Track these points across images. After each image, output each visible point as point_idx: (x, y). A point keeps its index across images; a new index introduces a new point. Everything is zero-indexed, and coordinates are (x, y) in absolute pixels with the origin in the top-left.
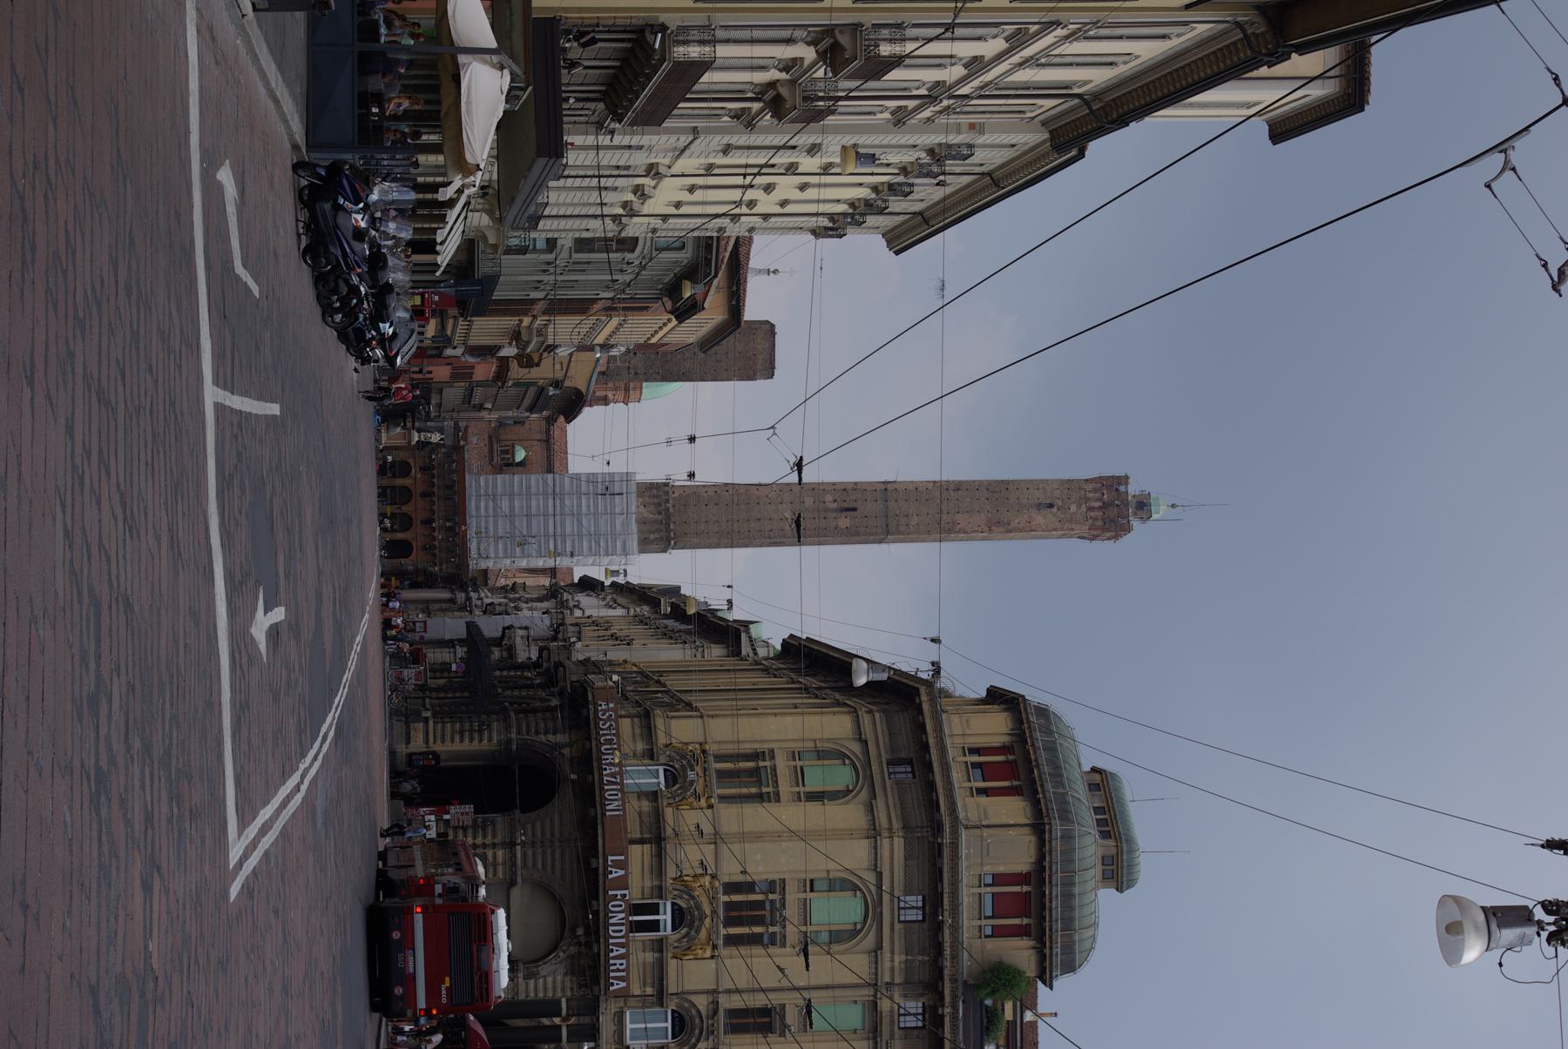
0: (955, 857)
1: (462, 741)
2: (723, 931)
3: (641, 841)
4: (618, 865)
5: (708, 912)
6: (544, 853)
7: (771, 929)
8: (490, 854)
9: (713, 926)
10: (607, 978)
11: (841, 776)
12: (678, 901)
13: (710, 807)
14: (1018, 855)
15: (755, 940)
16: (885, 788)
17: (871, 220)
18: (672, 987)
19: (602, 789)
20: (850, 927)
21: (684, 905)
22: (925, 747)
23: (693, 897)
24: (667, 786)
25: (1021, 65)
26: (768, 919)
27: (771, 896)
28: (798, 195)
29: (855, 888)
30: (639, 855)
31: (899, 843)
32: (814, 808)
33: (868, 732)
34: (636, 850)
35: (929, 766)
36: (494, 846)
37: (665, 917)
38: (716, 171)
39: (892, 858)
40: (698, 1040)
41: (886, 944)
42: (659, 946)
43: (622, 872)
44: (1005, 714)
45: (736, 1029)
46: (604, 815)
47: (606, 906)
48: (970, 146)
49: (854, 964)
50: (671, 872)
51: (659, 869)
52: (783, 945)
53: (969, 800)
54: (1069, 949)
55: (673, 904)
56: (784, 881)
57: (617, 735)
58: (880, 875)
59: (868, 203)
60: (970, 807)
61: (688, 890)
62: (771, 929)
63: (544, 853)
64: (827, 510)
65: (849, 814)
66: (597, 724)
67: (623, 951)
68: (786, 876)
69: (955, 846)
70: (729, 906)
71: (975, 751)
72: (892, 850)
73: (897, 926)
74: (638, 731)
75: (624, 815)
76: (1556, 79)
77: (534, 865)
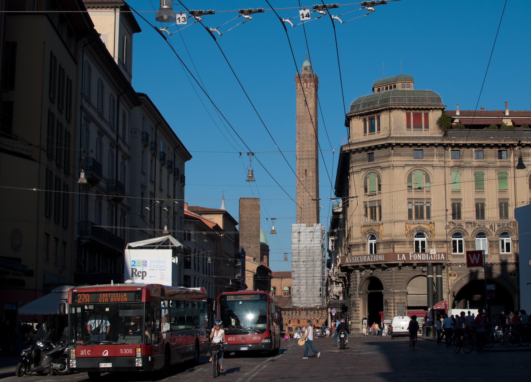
0: (400, 138)
1: (359, 310)
2: (425, 219)
3: (393, 248)
4: (401, 257)
5: (418, 225)
7: (425, 203)
8: (396, 301)
9: (424, 224)
10: (440, 260)
11: (373, 178)
12: (414, 235)
13: (382, 224)
14: (400, 116)
15: (428, 209)
16: (377, 163)
17: (178, 165)
18: (444, 238)
19: (375, 262)
20: (424, 176)
21: (416, 233)
22: (364, 149)
23: (413, 231)
24: (375, 239)
25: (101, 116)
26: (422, 204)
27: (413, 203)
28: (165, 192)
30: (398, 249)
31: (396, 158)
33: (359, 168)
34: (396, 250)
35: (370, 148)
36: (394, 299)
37: (420, 239)
38: (153, 220)
39: (400, 161)
40: (463, 229)
41: (430, 163)
42: (430, 242)
43: (404, 255)
45: (483, 217)
47: (415, 261)
48: (143, 133)
49: (437, 175)
50: (404, 238)
51: (403, 242)
53: (381, 133)
54: (432, 100)
55: (416, 237)
56: (475, 199)
57: (357, 256)
58: (407, 165)
59: (169, 167)
60: (383, 134)
61: (411, 232)
62: (425, 203)
63: (397, 282)
64: (306, 180)
65: (385, 175)
66: (353, 263)
68: (406, 198)
69: (396, 138)
70: (417, 217)
71: (365, 132)
73: (424, 159)
74: (356, 249)
75: (384, 254)
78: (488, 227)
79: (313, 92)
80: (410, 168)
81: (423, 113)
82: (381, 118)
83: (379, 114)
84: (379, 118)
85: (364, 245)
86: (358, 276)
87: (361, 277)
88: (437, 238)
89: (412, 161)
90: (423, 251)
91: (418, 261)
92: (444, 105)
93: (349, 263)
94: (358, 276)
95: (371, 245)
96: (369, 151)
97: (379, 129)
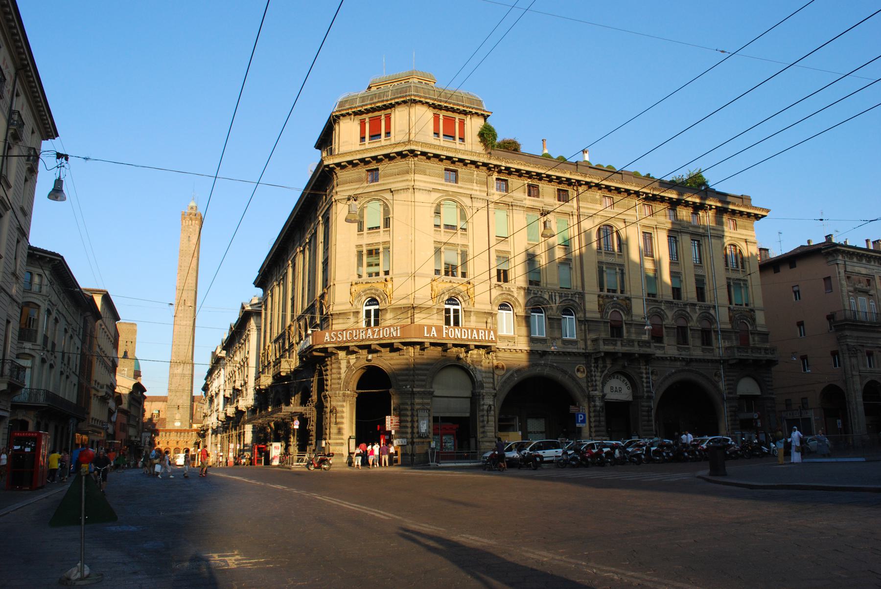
1: (342, 423)
4: (429, 331)
6: (418, 375)
8: (417, 407)
14: (423, 116)
21: (446, 297)
22: (363, 160)
29: (439, 205)
31: (418, 177)
32: (394, 223)
36: (412, 404)
39: (425, 182)
41: (469, 192)
43: (434, 329)
44: (341, 123)
46: (399, 338)
47: (451, 339)
50: (430, 303)
52: (467, 246)
58: (435, 190)
63: (418, 375)
67: (475, 331)
72: (421, 181)
76: (86, 159)
77: (423, 380)
78: (546, 297)
79: (198, 230)
80: (438, 195)
81: (457, 117)
82: (392, 117)
83: (388, 111)
84: (388, 118)
85: (357, 313)
86: (344, 365)
87: (349, 367)
88: (478, 307)
89: (442, 184)
90: (456, 323)
91: (456, 339)
92: (485, 108)
93: (330, 343)
94: (344, 365)
95: (368, 313)
96: (371, 166)
97: (388, 133)
